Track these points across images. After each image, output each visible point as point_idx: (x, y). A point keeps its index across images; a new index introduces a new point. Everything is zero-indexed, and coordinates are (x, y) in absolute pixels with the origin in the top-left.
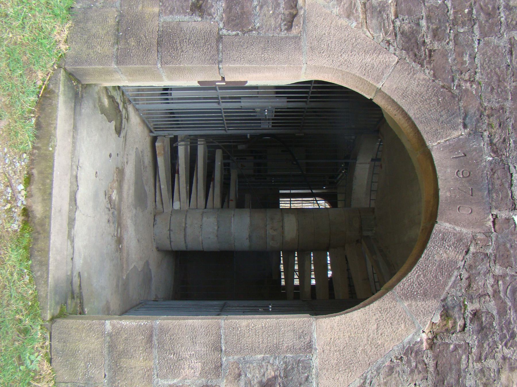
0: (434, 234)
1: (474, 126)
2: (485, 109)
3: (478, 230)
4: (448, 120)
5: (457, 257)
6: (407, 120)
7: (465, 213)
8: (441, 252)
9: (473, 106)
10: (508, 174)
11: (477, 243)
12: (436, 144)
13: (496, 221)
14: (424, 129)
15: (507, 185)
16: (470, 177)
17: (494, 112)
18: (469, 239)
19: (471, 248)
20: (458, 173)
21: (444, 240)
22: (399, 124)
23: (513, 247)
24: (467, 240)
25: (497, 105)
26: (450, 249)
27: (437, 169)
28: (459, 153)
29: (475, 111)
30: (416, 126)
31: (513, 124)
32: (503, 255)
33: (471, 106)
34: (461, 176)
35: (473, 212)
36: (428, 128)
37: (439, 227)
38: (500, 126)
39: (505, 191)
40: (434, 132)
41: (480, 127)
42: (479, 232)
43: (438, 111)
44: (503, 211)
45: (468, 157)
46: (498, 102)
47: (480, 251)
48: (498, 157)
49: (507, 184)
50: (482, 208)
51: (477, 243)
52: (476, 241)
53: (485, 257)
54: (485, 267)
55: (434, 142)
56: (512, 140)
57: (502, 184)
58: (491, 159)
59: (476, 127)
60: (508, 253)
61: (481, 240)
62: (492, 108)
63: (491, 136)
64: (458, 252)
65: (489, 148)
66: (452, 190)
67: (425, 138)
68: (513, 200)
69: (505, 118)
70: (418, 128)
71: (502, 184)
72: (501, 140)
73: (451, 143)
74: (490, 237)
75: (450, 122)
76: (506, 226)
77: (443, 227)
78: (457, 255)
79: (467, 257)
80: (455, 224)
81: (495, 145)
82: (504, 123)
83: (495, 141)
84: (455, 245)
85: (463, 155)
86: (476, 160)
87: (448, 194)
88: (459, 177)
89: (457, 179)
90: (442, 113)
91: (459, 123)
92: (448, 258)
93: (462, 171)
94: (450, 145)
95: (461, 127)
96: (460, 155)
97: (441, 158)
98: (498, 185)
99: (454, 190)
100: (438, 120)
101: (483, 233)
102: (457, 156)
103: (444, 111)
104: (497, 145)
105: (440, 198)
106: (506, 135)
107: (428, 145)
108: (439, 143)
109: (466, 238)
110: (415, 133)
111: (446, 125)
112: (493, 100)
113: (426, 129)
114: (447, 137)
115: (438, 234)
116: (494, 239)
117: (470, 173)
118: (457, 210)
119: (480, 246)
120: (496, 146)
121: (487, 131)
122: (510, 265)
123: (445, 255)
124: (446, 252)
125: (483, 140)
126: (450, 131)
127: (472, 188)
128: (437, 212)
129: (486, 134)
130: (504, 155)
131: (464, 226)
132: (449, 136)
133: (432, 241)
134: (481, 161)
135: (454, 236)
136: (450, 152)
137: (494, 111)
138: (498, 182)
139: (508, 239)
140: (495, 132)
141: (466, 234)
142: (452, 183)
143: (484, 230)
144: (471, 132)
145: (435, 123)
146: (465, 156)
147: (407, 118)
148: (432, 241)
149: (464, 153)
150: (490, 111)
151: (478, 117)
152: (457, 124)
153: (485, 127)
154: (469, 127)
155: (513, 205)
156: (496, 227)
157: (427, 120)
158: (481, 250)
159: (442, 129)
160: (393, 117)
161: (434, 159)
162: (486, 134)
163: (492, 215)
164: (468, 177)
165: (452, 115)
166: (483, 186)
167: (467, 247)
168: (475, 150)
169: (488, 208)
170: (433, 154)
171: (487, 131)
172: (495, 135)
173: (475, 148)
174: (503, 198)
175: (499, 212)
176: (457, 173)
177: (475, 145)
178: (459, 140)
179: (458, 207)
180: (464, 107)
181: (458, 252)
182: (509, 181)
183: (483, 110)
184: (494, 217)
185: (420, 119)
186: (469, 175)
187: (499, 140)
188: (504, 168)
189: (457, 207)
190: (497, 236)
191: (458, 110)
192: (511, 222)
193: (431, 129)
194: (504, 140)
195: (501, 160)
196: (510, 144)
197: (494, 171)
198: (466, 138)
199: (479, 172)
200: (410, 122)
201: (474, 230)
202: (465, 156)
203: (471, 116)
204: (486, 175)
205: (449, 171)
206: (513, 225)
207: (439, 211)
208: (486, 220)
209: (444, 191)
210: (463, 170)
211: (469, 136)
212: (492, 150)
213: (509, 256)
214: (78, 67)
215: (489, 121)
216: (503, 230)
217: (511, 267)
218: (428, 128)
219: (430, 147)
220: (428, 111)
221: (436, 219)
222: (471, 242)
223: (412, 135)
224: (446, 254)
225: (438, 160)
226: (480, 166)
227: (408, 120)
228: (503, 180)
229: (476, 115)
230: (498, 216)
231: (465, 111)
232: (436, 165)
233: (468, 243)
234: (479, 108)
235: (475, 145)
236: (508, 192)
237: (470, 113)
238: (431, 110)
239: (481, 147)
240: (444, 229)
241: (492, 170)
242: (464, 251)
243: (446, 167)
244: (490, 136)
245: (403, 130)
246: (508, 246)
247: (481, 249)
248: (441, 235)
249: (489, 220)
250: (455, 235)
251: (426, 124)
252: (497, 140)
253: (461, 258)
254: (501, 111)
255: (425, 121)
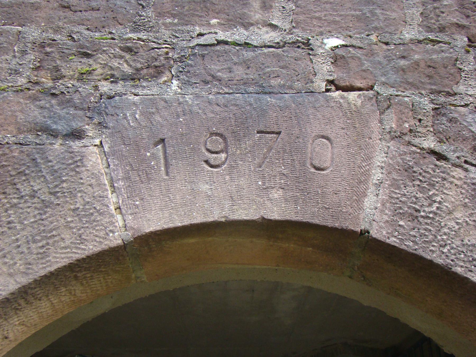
0: (401, 240)
1: (80, 113)
2: (37, 83)
3: (375, 124)
4: (49, 177)
5: (458, 183)
6: (28, 302)
7: (330, 155)
8: (452, 224)
9: (21, 111)
10: (218, 48)
11: (411, 131)
12: (119, 217)
13: (342, 84)
14: (65, 248)
15: (248, 54)
16: (226, 134)
17: (48, 65)
18: (403, 148)
19: (426, 145)
20: (212, 162)
21: (416, 214)
22: (39, 328)
23: (405, 54)
24: (405, 153)
25: (31, 57)
26: (438, 199)
27: (198, 219)
28: (154, 156)
29: (36, 106)
30: (52, 273)
31: (88, 29)
32: (430, 77)
33: (18, 114)
34: (223, 156)
35: (324, 134)
36: (66, 235)
37: (381, 227)
38: (87, 55)
39: (261, 59)
40: (81, 220)
41: (83, 99)
42: (381, 122)
43: (15, 201)
44: (315, 66)
45: (166, 133)
46: (24, 52)
47: (430, 124)
48: (171, 67)
49: (244, 53)
50: (311, 111)
51: (411, 131)
52: (405, 131)
53: (444, 115)
54: (470, 116)
55: (112, 223)
56: (130, 35)
57: (246, 64)
58: (175, 82)
59: (82, 109)
60: (422, 64)
61: (400, 121)
62: (37, 69)
63: (112, 76)
64: (444, 179)
65: (144, 84)
66: (264, 183)
67: (98, 249)
68: (284, 46)
69: (70, 43)
70: (60, 265)
71: (246, 64)
72: (128, 56)
73: (121, 175)
74: (389, 99)
75: (56, 171)
76: (353, 64)
77: (377, 214)
78: (451, 183)
79: (452, 156)
80: (365, 182)
81: (138, 70)
82: (82, 47)
83: (126, 69)
84: (425, 185)
85: (160, 147)
86: (178, 116)
87: (276, 194)
88: (224, 163)
89: (231, 167)
90: (25, 190)
91: (64, 148)
92: (465, 205)
93: (207, 154)
94: (127, 178)
95: (76, 145)
96: (161, 154)
97: (166, 206)
98: (248, 71)
99: (263, 177)
100: (46, 205)
101: (382, 113)
102: (162, 161)
103: (19, 186)
104: (139, 66)
105: (288, 218)
106: (116, 44)
107: (120, 242)
108: (118, 208)
109: (400, 155)
110: (76, 277)
111: (65, 185)
112: (14, 62)
113: (68, 242)
114: (100, 185)
115: (401, 230)
116: (392, 91)
117: (212, 134)
118: (322, 172)
119: (418, 124)
120: (142, 69)
121: (99, 84)
122: (452, 62)
123: (458, 214)
124: (450, 213)
125: (120, 95)
126: (84, 175)
127: (258, 132)
128: (334, 230)
129: (105, 87)
130: (167, 53)
131: (369, 158)
132: (98, 179)
133: (424, 249)
134: (180, 104)
135: (399, 188)
136: (149, 179)
137: (45, 64)
138: (239, 72)
139: (385, 62)
140: (105, 66)
141: (390, 155)
142: (243, 182)
143: (374, 111)
144: (96, 121)
145: (52, 215)
146: (163, 141)
147: (22, 302)
148: (424, 249)
149: (156, 144)
150: (42, 73)
151: (54, 102)
152: (68, 155)
153: (86, 89)
154: (80, 124)
155: (299, 47)
156: (358, 84)
157: (38, 238)
158: (428, 121)
159: (75, 196)
160: (13, 345)
161: (166, 227)
162: (105, 87)
163: (327, 90)
164: (225, 139)
165: (37, 164)
166: (251, 105)
167: (427, 155)
168: (147, 115)
169: (312, 99)
170: (151, 229)
171: (99, 84)
172: (111, 68)
173: (142, 114)
174: (282, 64)
175: (319, 76)
176: (212, 166)
177: (133, 115)
178: (113, 153)
179: (313, 170)
180: (20, 131)
181: (444, 179)
182: (237, 48)
183: (37, 88)
184: (333, 88)
185: (31, 258)
186: (221, 135)
187: (126, 61)
188: (203, 56)
189: (313, 174)
190: (384, 84)
191: (25, 148)
192: (340, 52)
193: (71, 228)
194: (129, 50)
195: (181, 62)
196: (139, 39)
197: (209, 78)
198: (112, 135)
199: (213, 112)
200: (38, 291)
201: (376, 135)
202: (163, 141)
203: (50, 117)
204: (220, 97)
205: (207, 186)
206: (351, 49)
207: (330, 223)
208: (345, 105)
209: (268, 204)
210: (204, 150)
211: (106, 127)
212: (153, 77)
213: (429, 64)
214: (265, 267)
215: (72, 78)
216: (364, 71)
217: (456, 60)
218: (66, 235)
219: (129, 236)
220: (9, 232)
221: (353, 233)
222: (409, 143)
223: (78, 290)
224: (454, 210)
225: (171, 214)
226: (195, 109)
227: (31, 299)
228: (235, 59)
229: (48, 105)
230: (331, 78)
231: (30, 131)
232: (186, 222)
233: (415, 153)
234: (30, 97)
235: (133, 115)
236: (265, 54)
237: (40, 119)
238: (9, 223)
239: (142, 102)
240: (382, 211)
241: (206, 83)
242: (438, 163)
243: (194, 193)
244: (113, 79)
245: (60, 316)
246: (402, 63)
247: (424, 123)
248: (401, 223)
249: (343, 97)
250: (395, 184)
251: (51, 241)
252: (126, 66)
253: (458, 173)
254: (48, 49)
255: (40, 244)
